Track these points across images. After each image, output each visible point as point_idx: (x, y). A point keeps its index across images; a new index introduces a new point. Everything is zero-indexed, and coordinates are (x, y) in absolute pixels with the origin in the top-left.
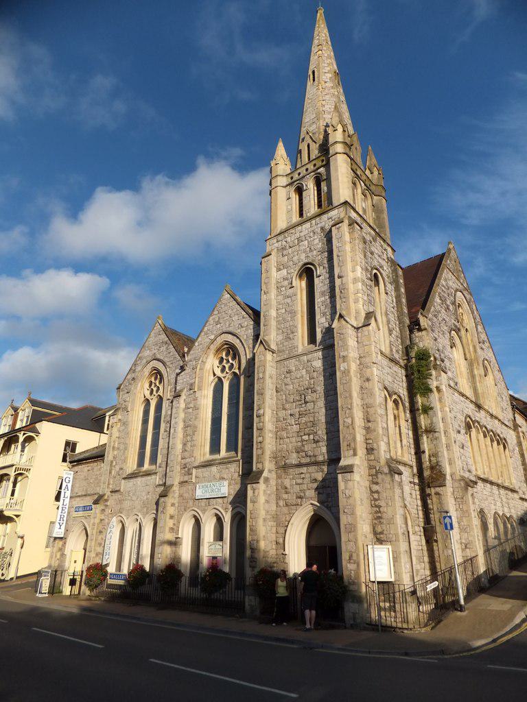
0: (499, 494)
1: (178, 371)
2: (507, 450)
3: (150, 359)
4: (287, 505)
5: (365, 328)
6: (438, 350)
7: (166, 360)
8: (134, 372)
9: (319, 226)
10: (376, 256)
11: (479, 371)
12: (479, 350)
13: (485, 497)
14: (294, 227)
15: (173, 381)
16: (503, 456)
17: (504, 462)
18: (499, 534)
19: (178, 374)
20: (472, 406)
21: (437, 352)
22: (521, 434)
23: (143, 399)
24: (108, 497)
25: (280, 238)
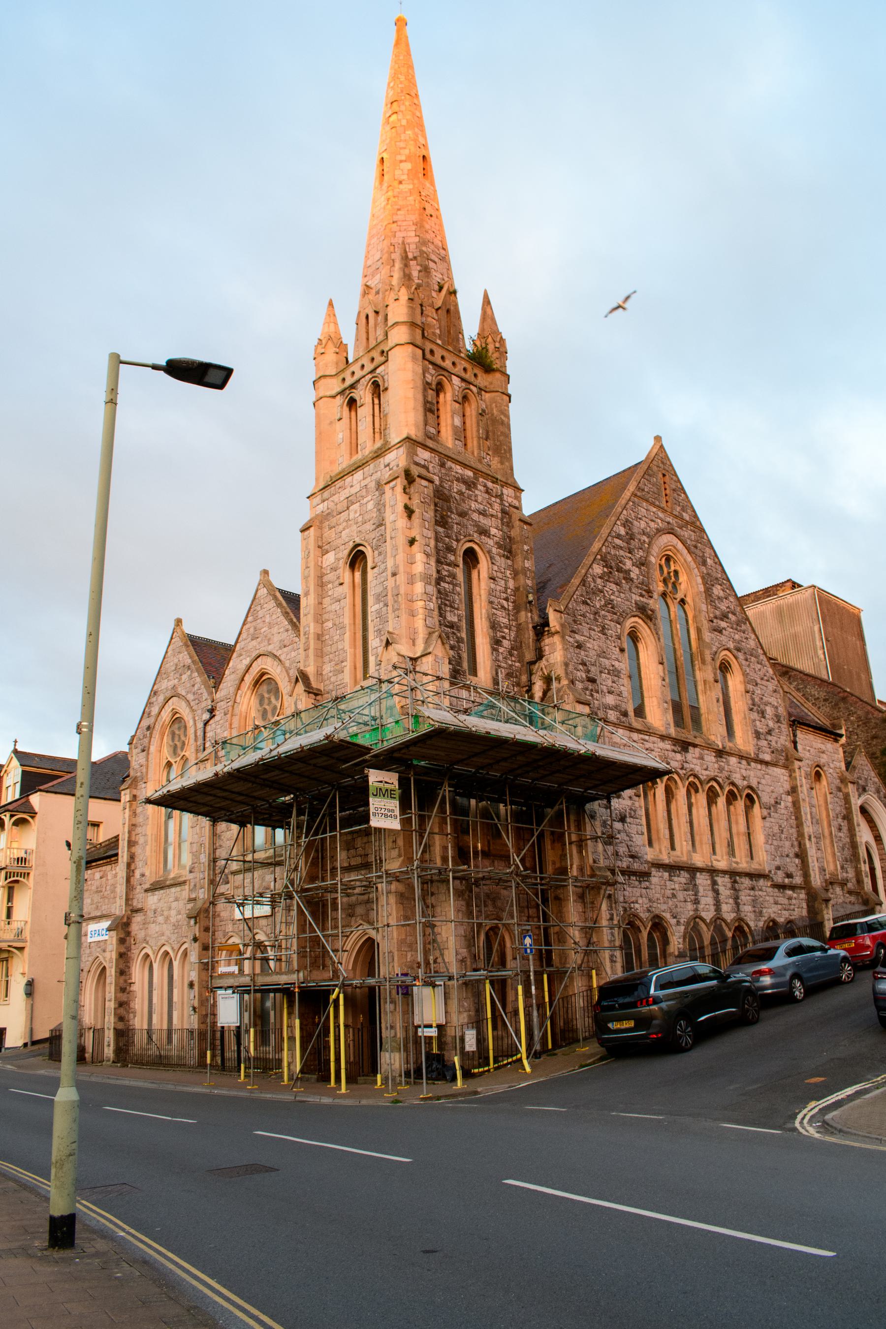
1: (206, 716)
2: (757, 806)
3: (168, 694)
5: (424, 659)
6: (584, 664)
7: (190, 697)
9: (374, 477)
10: (475, 516)
12: (707, 636)
13: (669, 893)
14: (342, 476)
15: (200, 733)
19: (206, 724)
23: (316, 330)
24: (128, 918)
25: (326, 494)
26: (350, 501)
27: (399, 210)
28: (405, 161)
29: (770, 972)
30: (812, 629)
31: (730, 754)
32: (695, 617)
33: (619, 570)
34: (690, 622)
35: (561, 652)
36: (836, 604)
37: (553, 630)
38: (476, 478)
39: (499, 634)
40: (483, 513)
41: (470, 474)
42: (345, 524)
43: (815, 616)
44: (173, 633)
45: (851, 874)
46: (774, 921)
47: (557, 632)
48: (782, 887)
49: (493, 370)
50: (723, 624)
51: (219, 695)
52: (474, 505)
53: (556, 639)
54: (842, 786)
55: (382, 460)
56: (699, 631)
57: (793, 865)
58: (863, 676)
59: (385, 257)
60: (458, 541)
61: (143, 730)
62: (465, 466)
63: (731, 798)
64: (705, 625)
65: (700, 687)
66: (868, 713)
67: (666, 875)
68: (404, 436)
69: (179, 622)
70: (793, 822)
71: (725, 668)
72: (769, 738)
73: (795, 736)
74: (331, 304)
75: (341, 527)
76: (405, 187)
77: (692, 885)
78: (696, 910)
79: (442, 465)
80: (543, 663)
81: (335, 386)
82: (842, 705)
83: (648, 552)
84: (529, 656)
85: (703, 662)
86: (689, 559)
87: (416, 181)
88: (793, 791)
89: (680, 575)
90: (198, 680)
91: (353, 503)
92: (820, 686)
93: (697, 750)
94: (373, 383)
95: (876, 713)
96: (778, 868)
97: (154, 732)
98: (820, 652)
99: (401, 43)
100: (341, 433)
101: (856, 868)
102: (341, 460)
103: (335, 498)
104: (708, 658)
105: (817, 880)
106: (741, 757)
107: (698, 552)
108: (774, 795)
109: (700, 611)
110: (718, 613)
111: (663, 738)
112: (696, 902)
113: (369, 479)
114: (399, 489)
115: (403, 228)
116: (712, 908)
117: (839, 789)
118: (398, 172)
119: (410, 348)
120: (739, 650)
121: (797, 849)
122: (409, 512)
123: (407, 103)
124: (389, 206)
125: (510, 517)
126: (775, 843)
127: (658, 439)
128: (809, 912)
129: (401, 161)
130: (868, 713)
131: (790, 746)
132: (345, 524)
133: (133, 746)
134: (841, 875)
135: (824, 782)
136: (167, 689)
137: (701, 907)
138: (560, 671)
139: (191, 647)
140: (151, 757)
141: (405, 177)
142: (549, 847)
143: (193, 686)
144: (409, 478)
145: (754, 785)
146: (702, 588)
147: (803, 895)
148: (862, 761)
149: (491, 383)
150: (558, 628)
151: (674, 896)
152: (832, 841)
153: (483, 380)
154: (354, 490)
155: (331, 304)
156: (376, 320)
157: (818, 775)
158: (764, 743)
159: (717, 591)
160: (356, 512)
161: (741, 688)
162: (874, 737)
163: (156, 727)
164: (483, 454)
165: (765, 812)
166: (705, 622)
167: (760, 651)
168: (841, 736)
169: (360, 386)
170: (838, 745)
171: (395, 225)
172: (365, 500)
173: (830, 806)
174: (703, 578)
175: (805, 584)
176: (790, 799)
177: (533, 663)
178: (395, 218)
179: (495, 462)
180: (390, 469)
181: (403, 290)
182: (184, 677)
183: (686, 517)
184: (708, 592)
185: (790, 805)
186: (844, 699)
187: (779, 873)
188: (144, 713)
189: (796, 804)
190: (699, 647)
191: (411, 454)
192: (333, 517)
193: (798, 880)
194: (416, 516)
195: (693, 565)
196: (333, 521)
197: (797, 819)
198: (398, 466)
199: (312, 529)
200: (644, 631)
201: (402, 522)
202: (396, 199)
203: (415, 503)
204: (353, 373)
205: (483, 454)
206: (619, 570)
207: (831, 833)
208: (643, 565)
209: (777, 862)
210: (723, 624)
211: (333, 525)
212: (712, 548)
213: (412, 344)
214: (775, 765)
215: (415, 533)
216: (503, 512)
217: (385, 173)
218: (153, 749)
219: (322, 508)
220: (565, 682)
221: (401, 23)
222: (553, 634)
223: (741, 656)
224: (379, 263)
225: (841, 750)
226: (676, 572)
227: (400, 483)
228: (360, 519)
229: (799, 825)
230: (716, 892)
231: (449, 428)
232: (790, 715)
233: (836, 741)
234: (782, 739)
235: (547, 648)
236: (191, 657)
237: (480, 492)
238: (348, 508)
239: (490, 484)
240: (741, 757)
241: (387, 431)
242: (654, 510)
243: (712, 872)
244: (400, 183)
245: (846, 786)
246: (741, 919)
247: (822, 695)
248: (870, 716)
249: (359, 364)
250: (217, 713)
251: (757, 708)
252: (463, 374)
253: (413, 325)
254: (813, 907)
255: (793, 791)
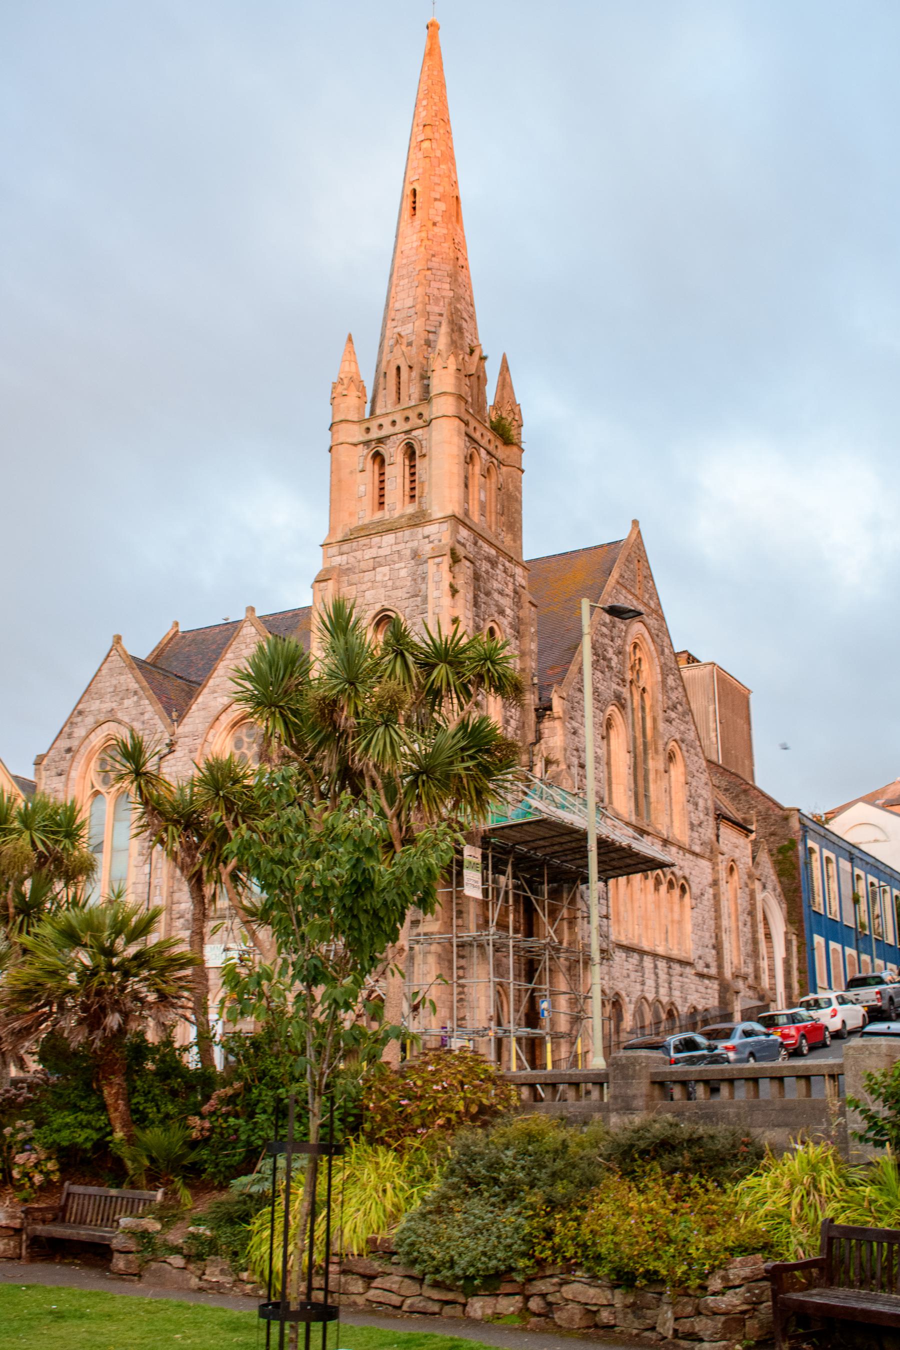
0: (656, 967)
2: (687, 895)
4: (505, 572)
6: (577, 750)
8: (70, 736)
9: (409, 545)
11: (655, 763)
12: (662, 726)
13: (625, 972)
16: (676, 908)
17: (676, 916)
18: (635, 747)
20: (630, 831)
21: (575, 753)
22: (701, 755)
25: (346, 547)
26: (377, 563)
27: (433, 256)
28: (440, 200)
29: (733, 1048)
30: (706, 708)
31: (672, 844)
32: (652, 706)
33: (604, 659)
34: (647, 710)
35: (562, 738)
36: (731, 685)
37: (556, 715)
38: (497, 557)
39: (509, 714)
40: (501, 593)
41: (493, 552)
42: (369, 584)
43: (711, 696)
44: (111, 650)
45: (750, 970)
46: (695, 1008)
47: (559, 718)
48: (701, 976)
49: (512, 444)
50: (673, 715)
51: (180, 730)
52: (496, 585)
53: (557, 724)
54: (749, 882)
55: (420, 529)
56: (654, 720)
57: (710, 955)
58: (747, 762)
59: (419, 307)
60: (484, 620)
61: (59, 751)
62: (491, 544)
63: (671, 885)
64: (661, 716)
65: (652, 776)
66: (768, 809)
67: (624, 955)
68: (449, 513)
69: (118, 639)
70: (713, 914)
71: (671, 758)
72: (700, 830)
73: (718, 829)
74: (350, 339)
75: (364, 587)
76: (440, 230)
77: (640, 968)
78: (642, 991)
79: (475, 544)
80: (542, 745)
81: (356, 434)
82: (743, 797)
83: (624, 641)
84: (531, 738)
85: (656, 751)
86: (653, 648)
87: (450, 226)
88: (715, 883)
89: (643, 662)
90: (150, 708)
91: (381, 566)
92: (722, 774)
93: (650, 838)
94: (407, 444)
95: (777, 810)
96: (700, 958)
97: (78, 756)
98: (713, 734)
99: (433, 52)
100: (365, 484)
101: (755, 963)
102: (361, 514)
103: (358, 554)
104: (661, 748)
105: (728, 974)
106: (680, 848)
107: (659, 641)
108: (701, 887)
109: (657, 701)
110: (670, 703)
111: (628, 824)
112: (643, 983)
113: (402, 546)
114: (445, 566)
115: (438, 278)
116: (654, 990)
117: (747, 886)
118: (432, 212)
119: (457, 421)
120: (683, 741)
121: (714, 941)
122: (454, 591)
123: (442, 131)
124: (423, 249)
125: (520, 597)
126: (699, 933)
127: (635, 523)
128: (720, 1002)
129: (436, 199)
130: (768, 809)
131: (714, 838)
132: (369, 584)
133: (42, 767)
134: (744, 970)
135: (736, 876)
136: (99, 710)
137: (646, 988)
138: (557, 755)
139: (137, 671)
140: (70, 784)
141: (439, 219)
142: (545, 920)
143: (142, 714)
144: (455, 559)
145: (687, 875)
146: (659, 678)
147: (715, 985)
148: (764, 858)
149: (508, 457)
150: (561, 715)
151: (628, 976)
152: (738, 936)
153: (502, 452)
154: (382, 552)
155: (350, 339)
156: (410, 376)
157: (731, 869)
158: (696, 835)
159: (671, 681)
160: (385, 575)
161: (682, 779)
162: (773, 834)
163: (82, 750)
164: (499, 531)
165: (694, 902)
166: (660, 712)
167: (698, 743)
168: (751, 832)
169: (390, 442)
170: (748, 840)
171: (429, 272)
172: (397, 566)
173: (739, 901)
174: (661, 668)
175: (704, 659)
176: (711, 891)
177: (534, 744)
178: (430, 265)
179: (508, 539)
180: (430, 542)
181: (452, 359)
182: (127, 703)
183: (652, 605)
184: (664, 682)
185: (711, 897)
186: (745, 791)
187: (701, 962)
188: (61, 732)
189: (716, 897)
190: (654, 736)
191: (455, 532)
192: (354, 573)
193: (713, 971)
194: (460, 596)
195: (655, 654)
196: (355, 578)
197: (716, 911)
198: (440, 541)
199: (330, 582)
200: (618, 720)
201: (447, 600)
202: (430, 243)
203: (460, 583)
204: (381, 426)
205: (499, 531)
206: (604, 659)
207: (738, 928)
208: (620, 653)
209: (699, 953)
210: (673, 715)
211: (354, 581)
212: (669, 637)
213: (459, 417)
214: (703, 857)
215: (460, 612)
216: (515, 592)
217: (418, 205)
218: (74, 774)
219: (338, 560)
220: (563, 766)
221: (432, 27)
222: (554, 719)
223: (683, 746)
224: (412, 311)
225: (750, 846)
226: (640, 660)
227: (447, 561)
228: (390, 583)
229: (718, 917)
230: (656, 974)
231: (476, 502)
232: (716, 809)
233: (747, 836)
234: (708, 832)
235: (546, 731)
236: (138, 682)
237: (499, 571)
238: (374, 569)
239: (507, 564)
240: (680, 848)
241: (424, 500)
242: (630, 597)
243: (655, 955)
244: (434, 224)
245: (753, 882)
246: (672, 1004)
247: (724, 784)
248: (770, 812)
249: (390, 418)
250: (176, 747)
251: (692, 800)
252: (488, 447)
253: (460, 397)
254: (725, 998)
255: (715, 883)
